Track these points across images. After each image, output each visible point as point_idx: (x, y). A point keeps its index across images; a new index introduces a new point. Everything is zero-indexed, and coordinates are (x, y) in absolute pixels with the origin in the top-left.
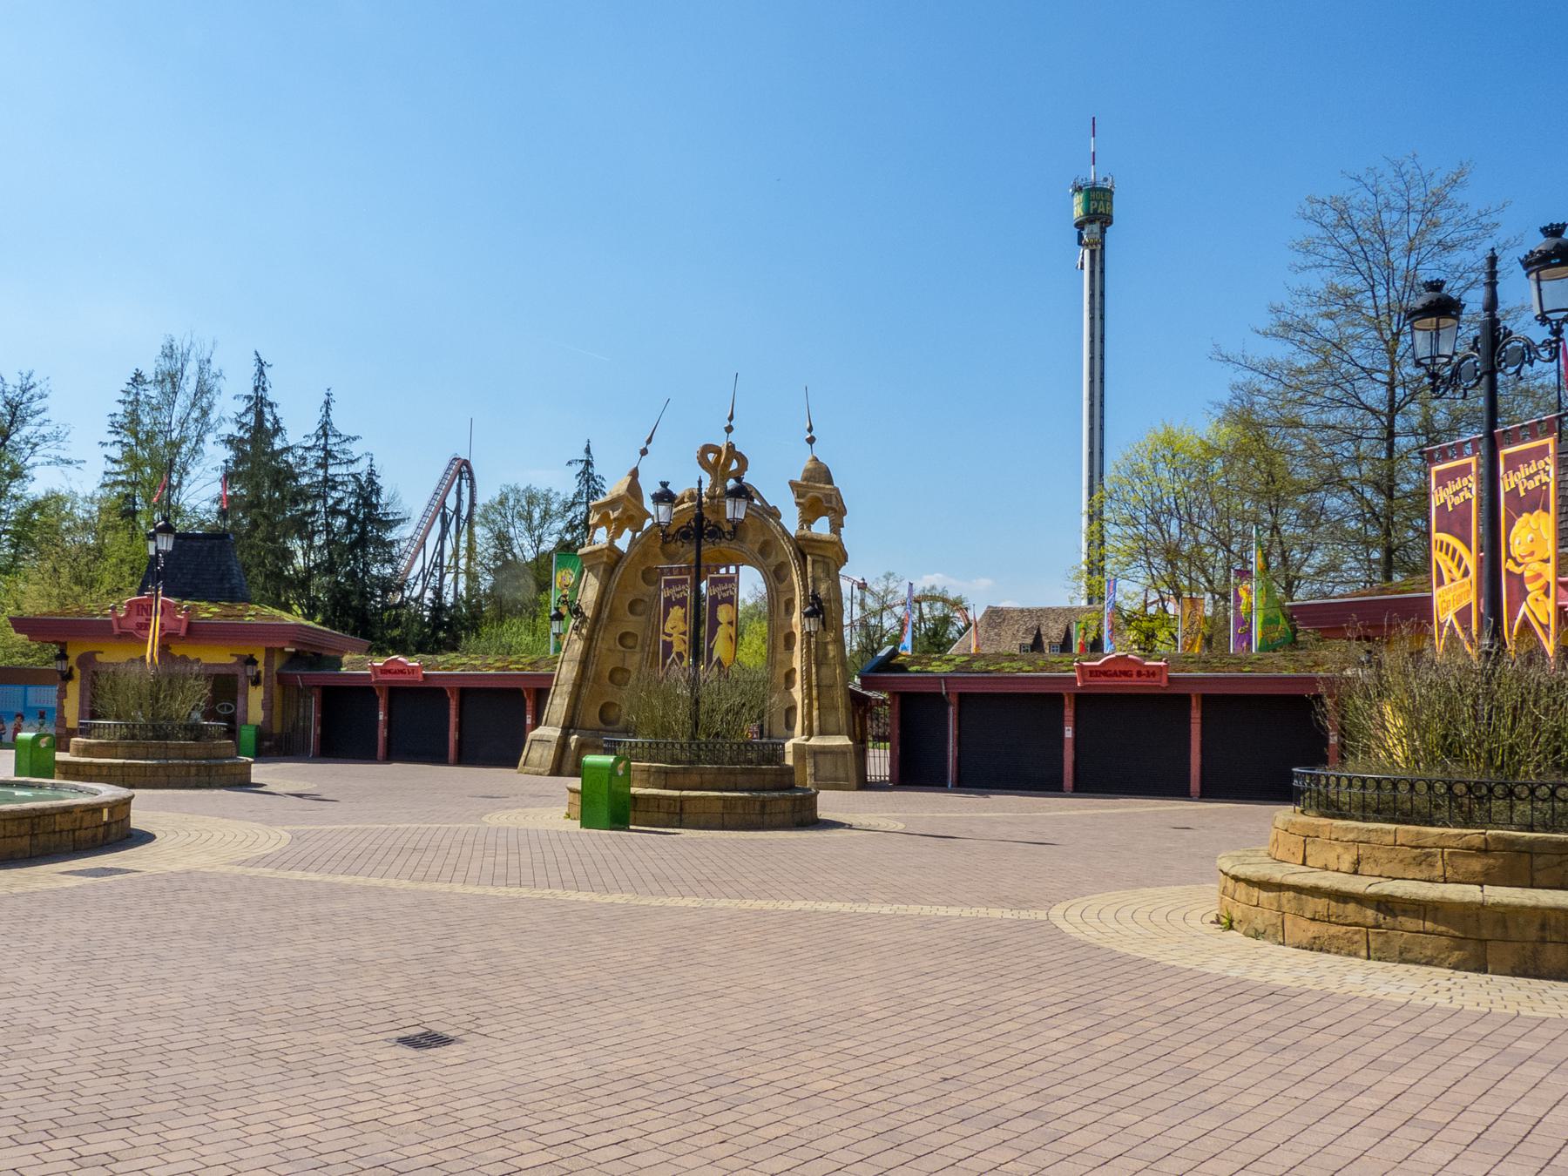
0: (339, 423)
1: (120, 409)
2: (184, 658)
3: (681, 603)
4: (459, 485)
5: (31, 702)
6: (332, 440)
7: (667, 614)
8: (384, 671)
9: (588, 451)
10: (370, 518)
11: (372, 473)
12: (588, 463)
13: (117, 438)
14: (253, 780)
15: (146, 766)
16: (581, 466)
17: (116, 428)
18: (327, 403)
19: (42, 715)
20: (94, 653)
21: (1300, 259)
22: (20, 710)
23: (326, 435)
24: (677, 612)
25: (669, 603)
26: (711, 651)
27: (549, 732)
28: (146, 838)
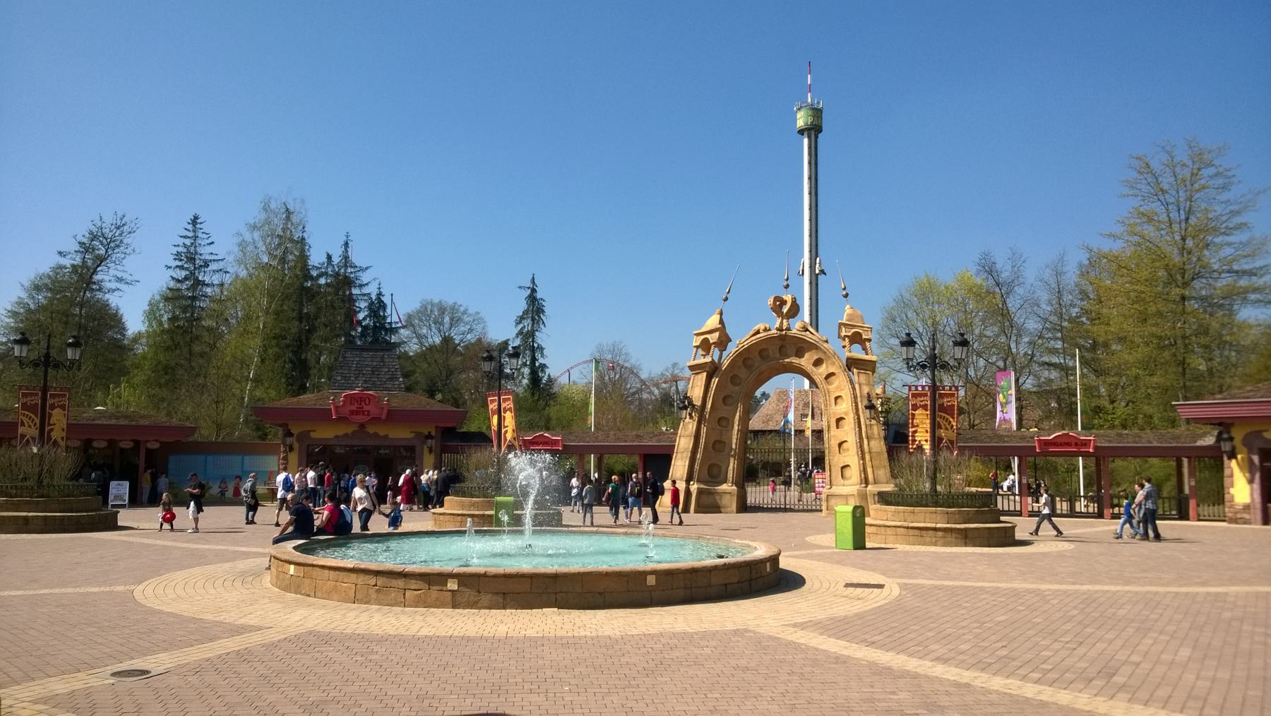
2: (376, 435)
9: (533, 281)
10: (383, 327)
11: (380, 294)
12: (534, 291)
13: (180, 263)
14: (120, 524)
17: (178, 256)
18: (346, 244)
21: (1127, 191)
22: (239, 473)
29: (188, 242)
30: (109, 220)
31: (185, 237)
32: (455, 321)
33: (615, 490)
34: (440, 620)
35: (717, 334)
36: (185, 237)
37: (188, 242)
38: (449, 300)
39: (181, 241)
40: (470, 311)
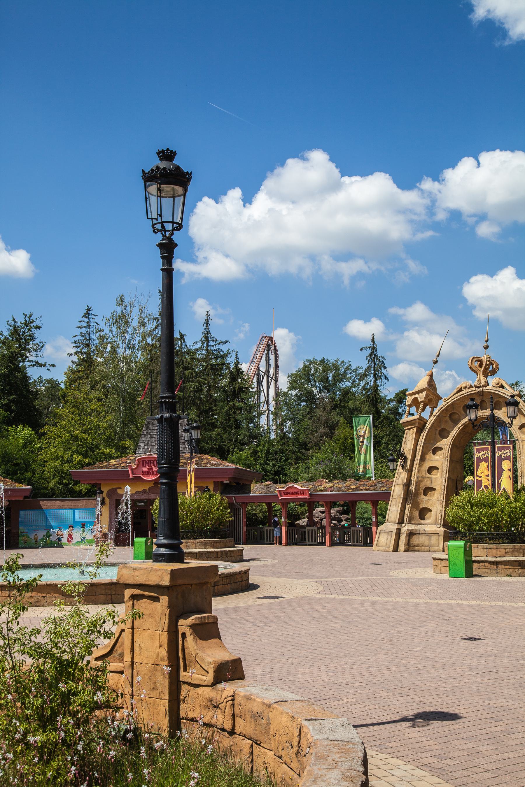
0: (215, 333)
1: (78, 331)
3: (486, 460)
4: (268, 355)
5: (77, 519)
6: (211, 343)
7: (478, 466)
8: (286, 493)
12: (374, 349)
13: (79, 350)
15: (217, 552)
16: (369, 351)
19: (83, 525)
20: (116, 489)
23: (207, 341)
24: (483, 465)
25: (479, 460)
26: (499, 485)
27: (390, 526)
28: (255, 587)
29: (84, 330)
30: (21, 319)
31: (81, 327)
32: (339, 378)
33: (52, 698)
34: (226, 782)
35: (424, 394)
36: (81, 327)
37: (84, 330)
38: (331, 358)
39: (79, 331)
40: (353, 367)
